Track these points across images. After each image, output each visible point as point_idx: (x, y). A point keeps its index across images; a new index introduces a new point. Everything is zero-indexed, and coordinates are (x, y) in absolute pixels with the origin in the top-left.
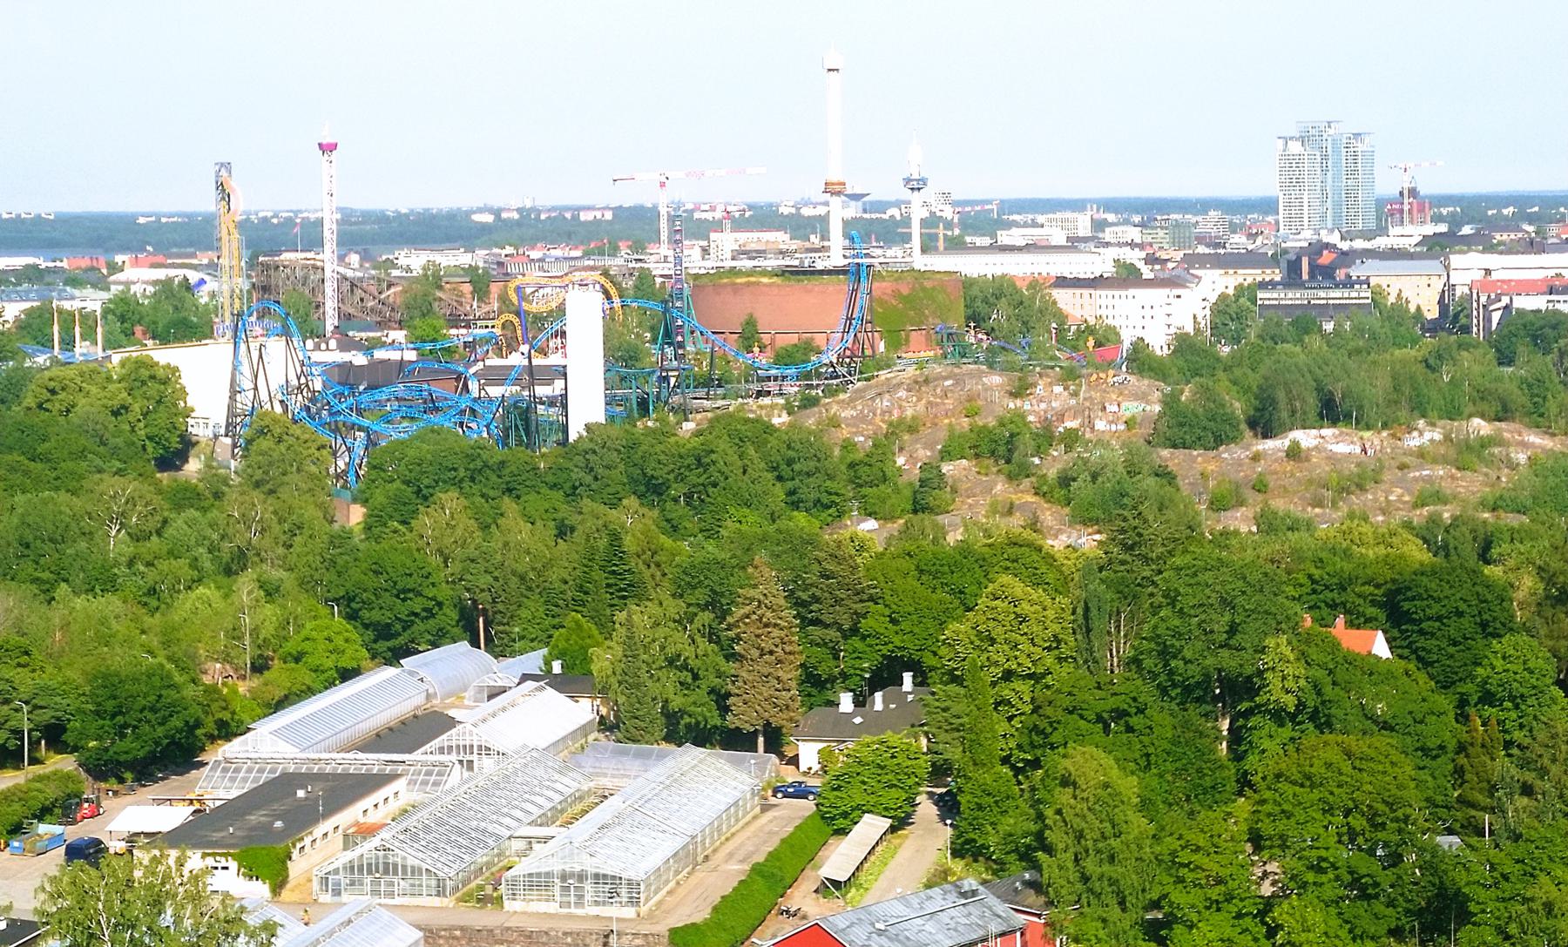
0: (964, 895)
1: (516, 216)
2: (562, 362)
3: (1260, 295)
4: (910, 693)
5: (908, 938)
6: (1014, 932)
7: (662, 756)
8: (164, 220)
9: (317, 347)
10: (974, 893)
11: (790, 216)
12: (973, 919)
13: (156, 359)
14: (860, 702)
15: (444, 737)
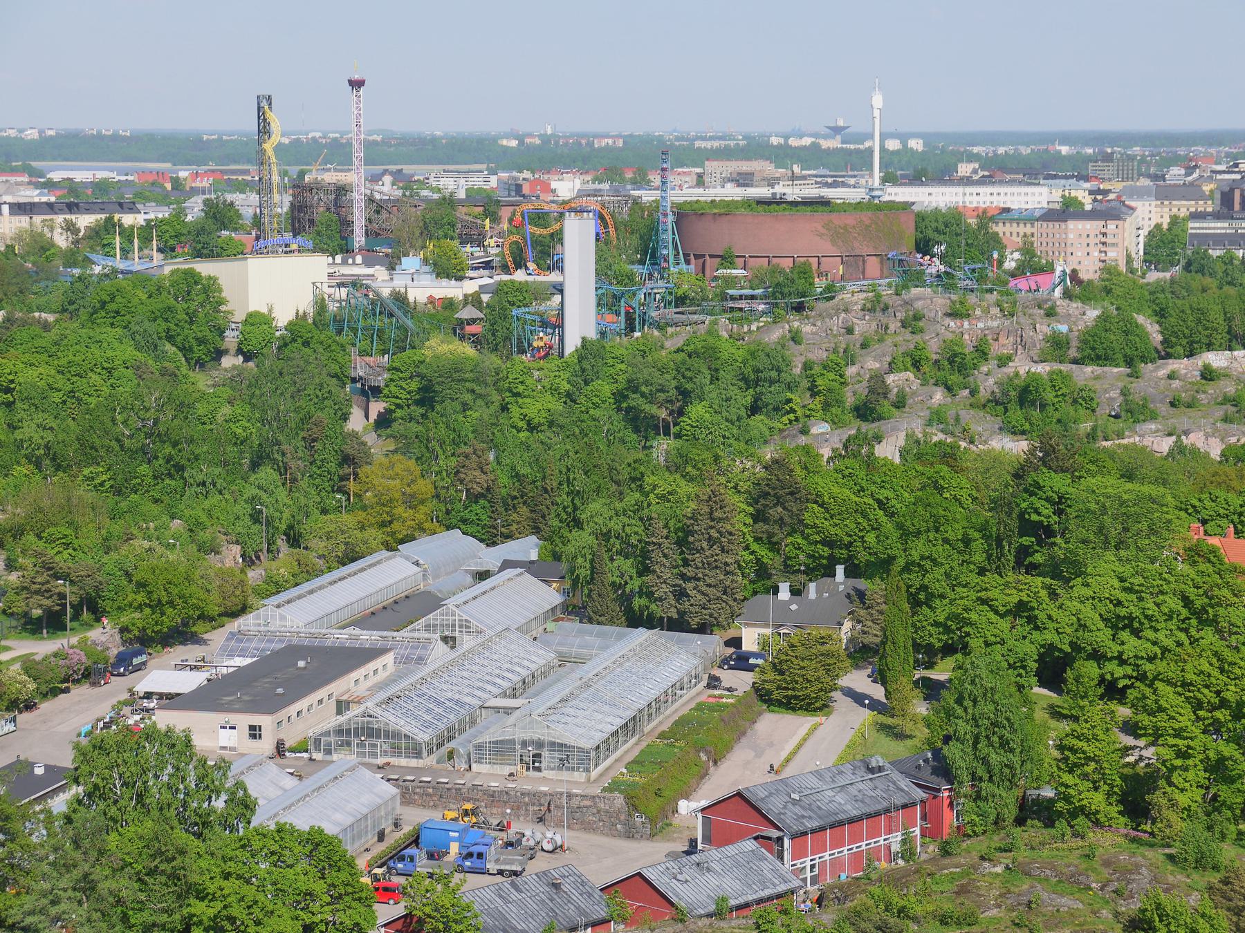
0: (871, 770)
1: (538, 141)
2: (560, 279)
3: (1191, 225)
4: (841, 584)
5: (819, 808)
6: (914, 804)
7: (620, 637)
8: (224, 138)
9: (344, 263)
10: (880, 769)
11: (779, 146)
12: (879, 792)
13: (198, 270)
14: (795, 592)
15: (430, 616)
